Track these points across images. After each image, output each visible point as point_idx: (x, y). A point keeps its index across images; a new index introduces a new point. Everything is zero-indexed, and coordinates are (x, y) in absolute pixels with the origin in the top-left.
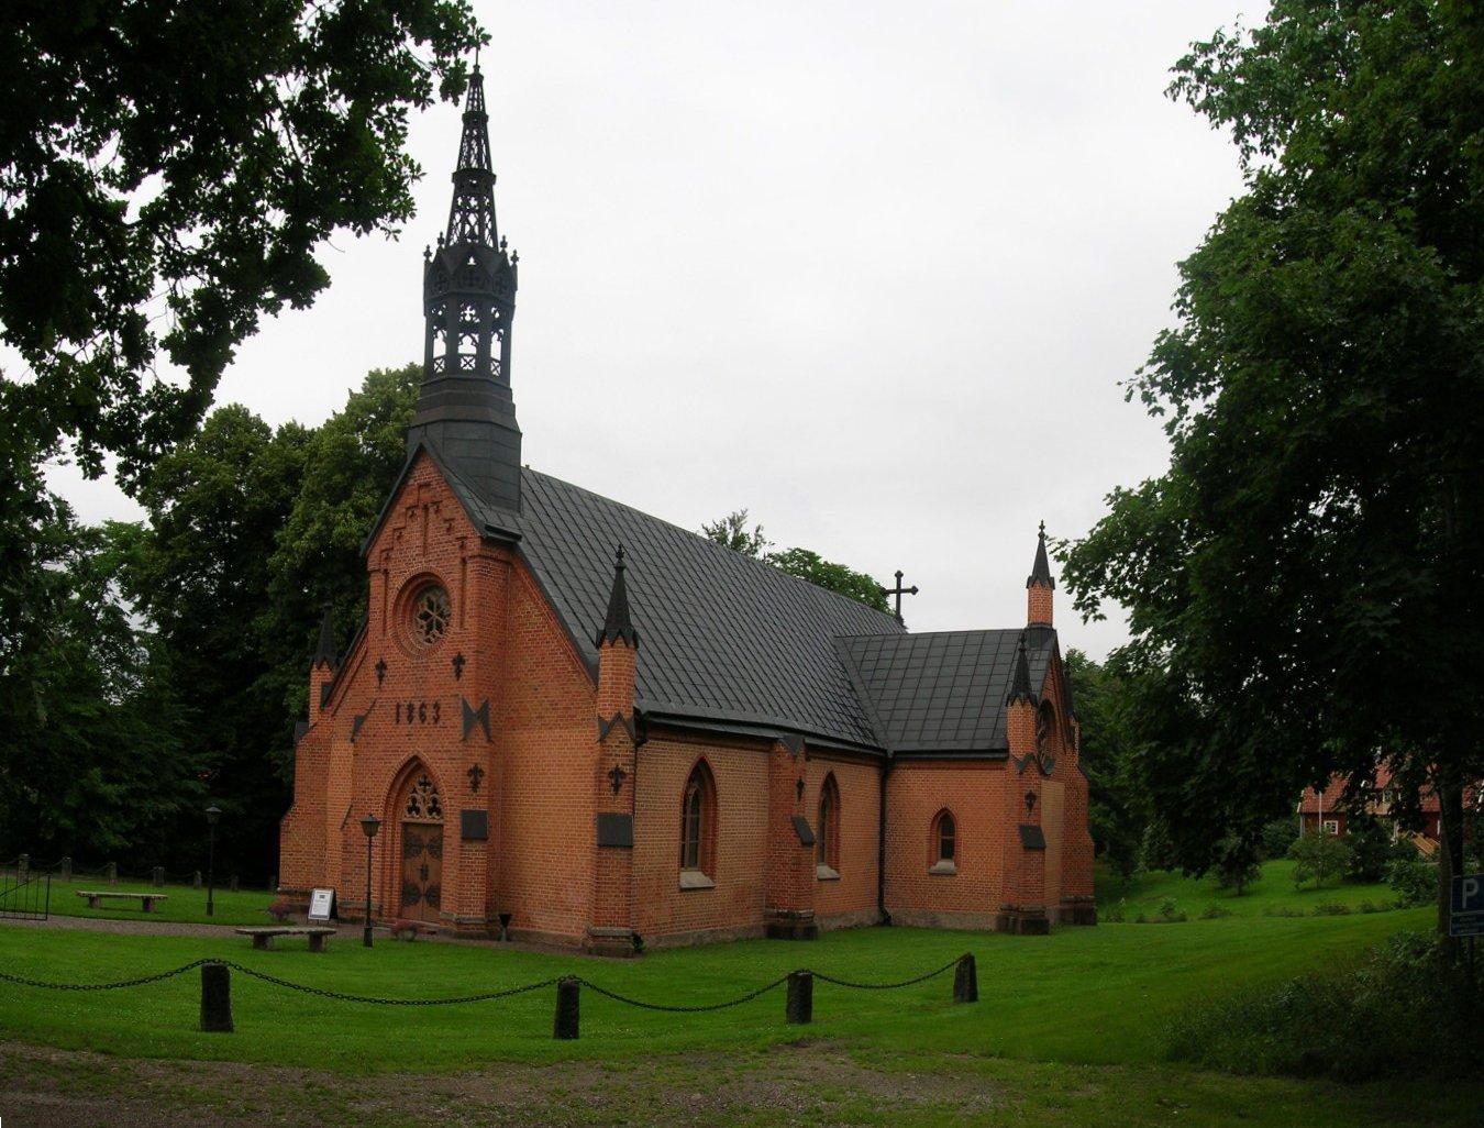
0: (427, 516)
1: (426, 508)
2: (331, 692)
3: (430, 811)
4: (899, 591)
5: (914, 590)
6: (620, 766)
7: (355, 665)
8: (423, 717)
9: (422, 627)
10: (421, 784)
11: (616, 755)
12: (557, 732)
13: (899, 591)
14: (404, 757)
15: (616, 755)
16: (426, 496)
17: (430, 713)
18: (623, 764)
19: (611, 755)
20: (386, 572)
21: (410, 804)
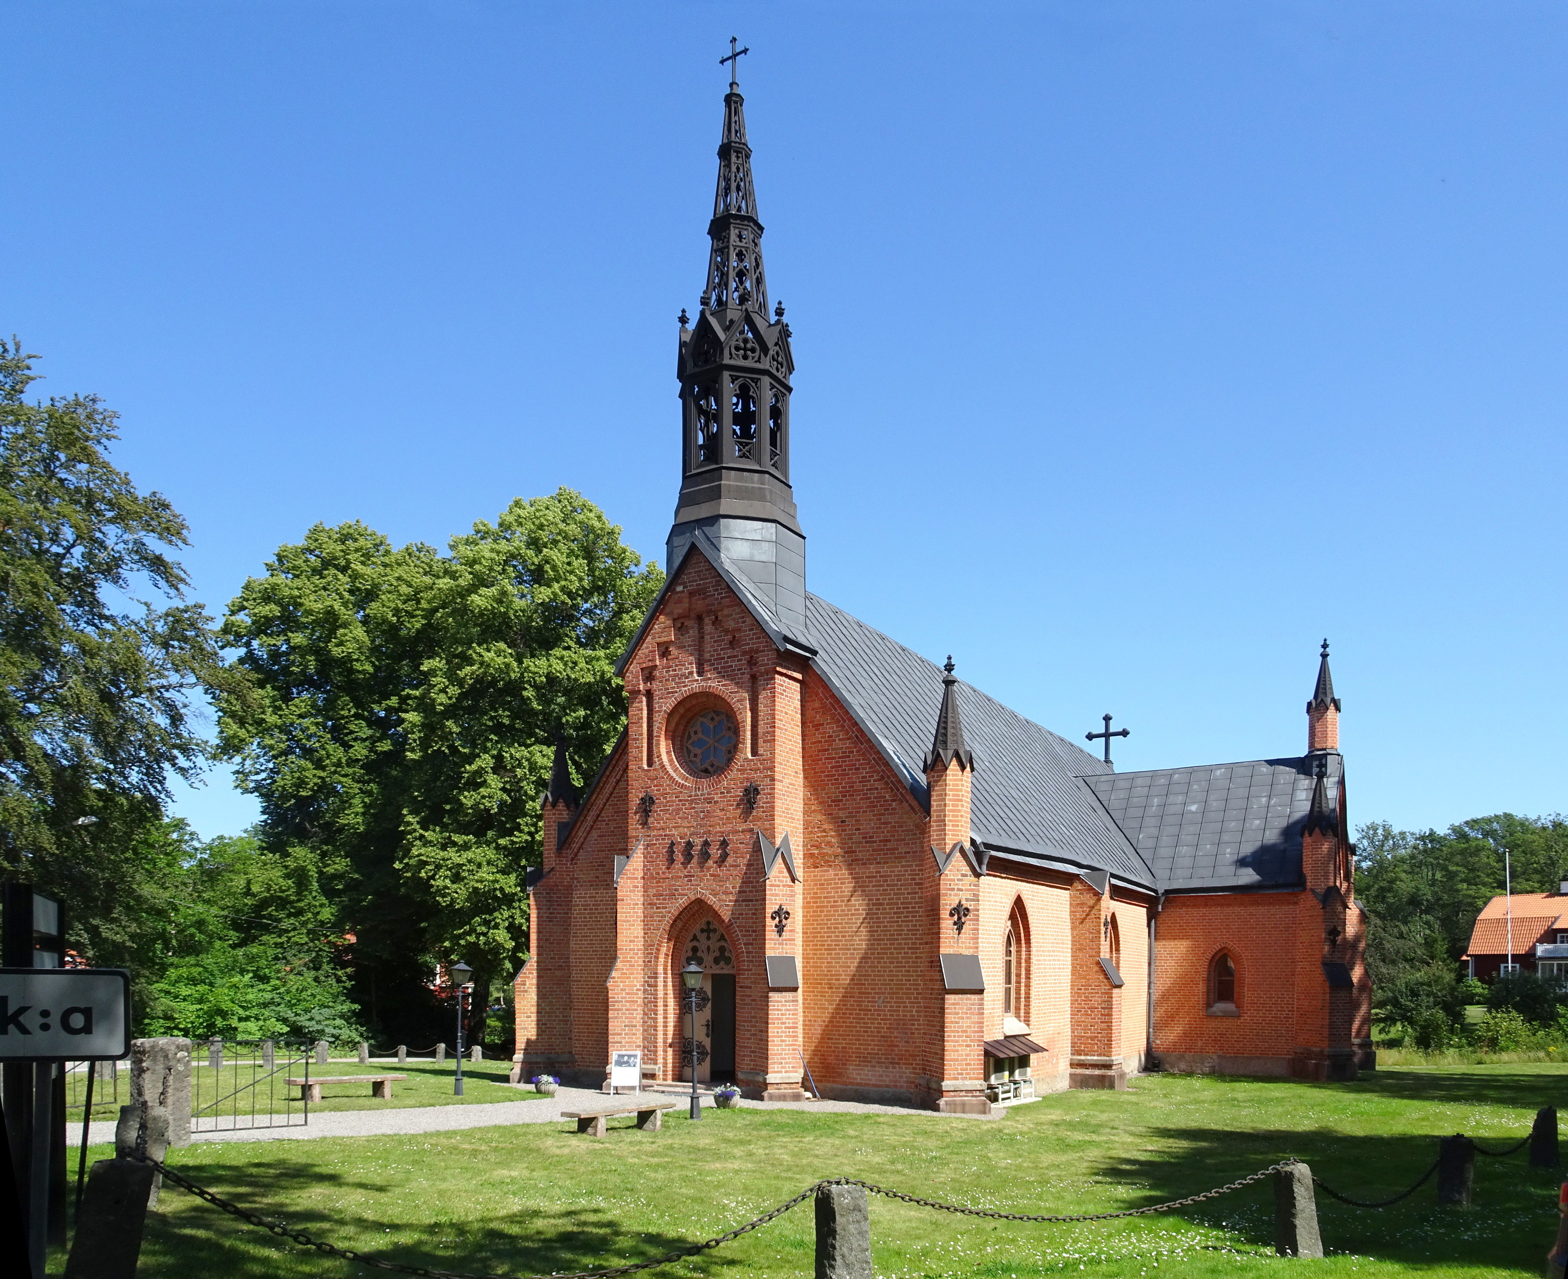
0: (701, 628)
1: (700, 618)
2: (570, 833)
3: (716, 961)
4: (1107, 735)
5: (1125, 733)
6: (963, 902)
7: (600, 802)
8: (705, 856)
9: (695, 756)
10: (702, 931)
11: (959, 890)
12: (872, 868)
13: (1107, 735)
14: (682, 902)
15: (959, 890)
16: (699, 605)
17: (715, 852)
18: (967, 900)
19: (953, 889)
20: (649, 694)
21: (690, 954)
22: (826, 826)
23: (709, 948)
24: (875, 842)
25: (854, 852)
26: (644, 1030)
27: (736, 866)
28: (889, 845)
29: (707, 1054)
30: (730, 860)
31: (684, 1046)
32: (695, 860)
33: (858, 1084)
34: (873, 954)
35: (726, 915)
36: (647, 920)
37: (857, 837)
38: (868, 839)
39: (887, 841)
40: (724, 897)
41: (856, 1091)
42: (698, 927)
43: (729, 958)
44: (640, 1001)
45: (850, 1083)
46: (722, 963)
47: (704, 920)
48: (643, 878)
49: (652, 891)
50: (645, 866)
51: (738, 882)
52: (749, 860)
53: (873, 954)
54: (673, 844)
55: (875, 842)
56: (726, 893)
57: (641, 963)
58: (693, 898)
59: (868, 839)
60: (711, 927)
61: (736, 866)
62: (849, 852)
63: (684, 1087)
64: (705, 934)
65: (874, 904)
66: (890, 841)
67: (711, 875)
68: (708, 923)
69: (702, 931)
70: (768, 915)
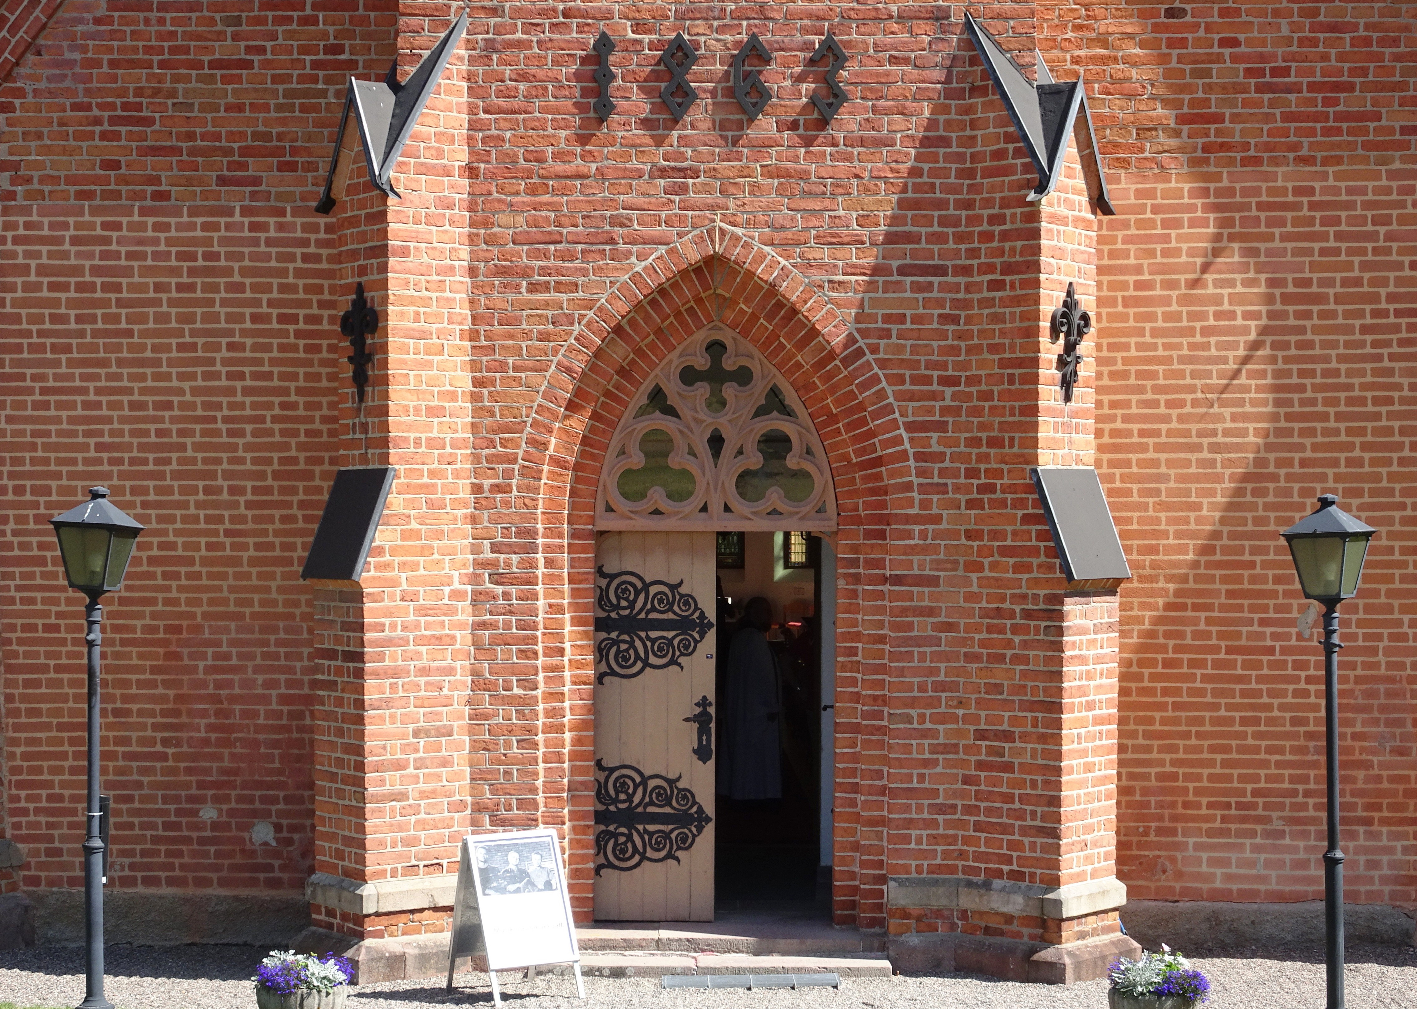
10: (689, 376)
12: (1284, 177)
14: (645, 266)
17: (787, 86)
22: (1106, 25)
23: (716, 442)
24: (1295, 88)
25: (1218, 118)
26: (476, 746)
27: (879, 143)
28: (1345, 103)
29: (702, 819)
30: (848, 120)
31: (601, 794)
32: (700, 115)
33: (1216, 895)
34: (1281, 463)
35: (833, 320)
36: (485, 332)
37: (1226, 70)
38: (1269, 77)
39: (1337, 87)
40: (825, 254)
41: (1214, 919)
42: (675, 361)
43: (803, 475)
44: (463, 637)
45: (1185, 892)
46: (657, 497)
47: (701, 337)
48: (471, 171)
49: (508, 224)
50: (473, 126)
51: (885, 205)
52: (932, 124)
53: (1281, 463)
54: (605, 45)
55: (1295, 88)
56: (833, 241)
57: (465, 494)
58: (694, 256)
59: (1269, 77)
60: (729, 364)
61: (879, 143)
62: (1195, 118)
63: (659, 945)
64: (702, 390)
65: (1286, 298)
66: (1350, 88)
67: (769, 172)
68: (716, 348)
69: (689, 376)
70: (1045, 324)
